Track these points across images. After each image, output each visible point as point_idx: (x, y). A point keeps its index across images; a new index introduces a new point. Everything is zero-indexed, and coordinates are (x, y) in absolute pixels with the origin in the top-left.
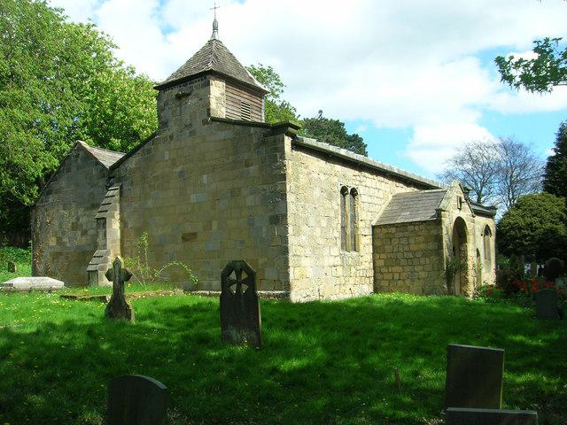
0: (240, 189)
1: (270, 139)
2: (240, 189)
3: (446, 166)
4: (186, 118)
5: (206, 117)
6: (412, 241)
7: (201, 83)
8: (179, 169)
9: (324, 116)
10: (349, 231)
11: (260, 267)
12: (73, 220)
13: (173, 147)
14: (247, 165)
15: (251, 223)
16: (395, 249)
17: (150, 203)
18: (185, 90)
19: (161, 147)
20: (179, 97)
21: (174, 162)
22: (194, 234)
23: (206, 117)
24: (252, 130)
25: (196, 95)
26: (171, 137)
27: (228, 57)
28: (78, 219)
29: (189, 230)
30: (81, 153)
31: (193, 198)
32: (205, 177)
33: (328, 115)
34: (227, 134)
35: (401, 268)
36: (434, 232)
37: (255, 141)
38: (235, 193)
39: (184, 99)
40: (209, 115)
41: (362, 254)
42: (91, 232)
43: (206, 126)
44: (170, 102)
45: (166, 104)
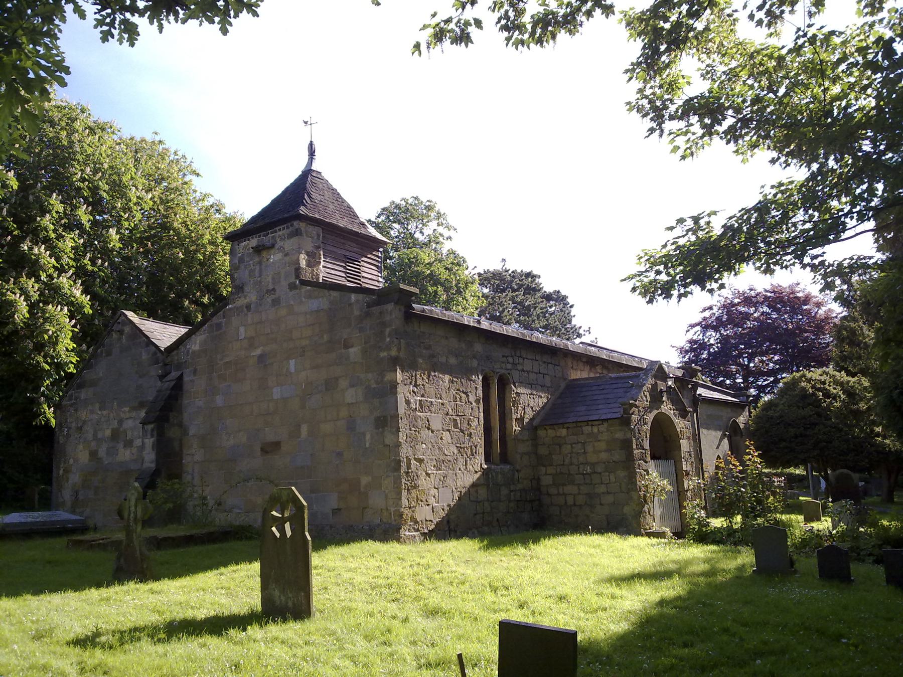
0: (337, 379)
1: (376, 310)
2: (337, 379)
3: (690, 335)
4: (268, 279)
5: (293, 279)
6: (589, 448)
7: (286, 232)
8: (258, 352)
9: (508, 267)
10: (496, 435)
11: (362, 489)
12: (115, 424)
13: (250, 321)
14: (347, 346)
15: (351, 426)
16: (567, 461)
17: (219, 400)
18: (266, 240)
19: (235, 321)
20: (258, 250)
21: (252, 343)
22: (277, 445)
23: (293, 279)
24: (353, 297)
25: (281, 249)
26: (248, 307)
27: (245, 228)
28: (121, 422)
29: (270, 436)
30: (127, 329)
31: (277, 393)
32: (292, 362)
33: (512, 266)
34: (321, 302)
35: (576, 488)
36: (619, 435)
37: (357, 313)
38: (330, 385)
39: (264, 254)
40: (297, 276)
41: (518, 467)
42: (138, 442)
43: (293, 292)
44: (246, 259)
45: (241, 260)
